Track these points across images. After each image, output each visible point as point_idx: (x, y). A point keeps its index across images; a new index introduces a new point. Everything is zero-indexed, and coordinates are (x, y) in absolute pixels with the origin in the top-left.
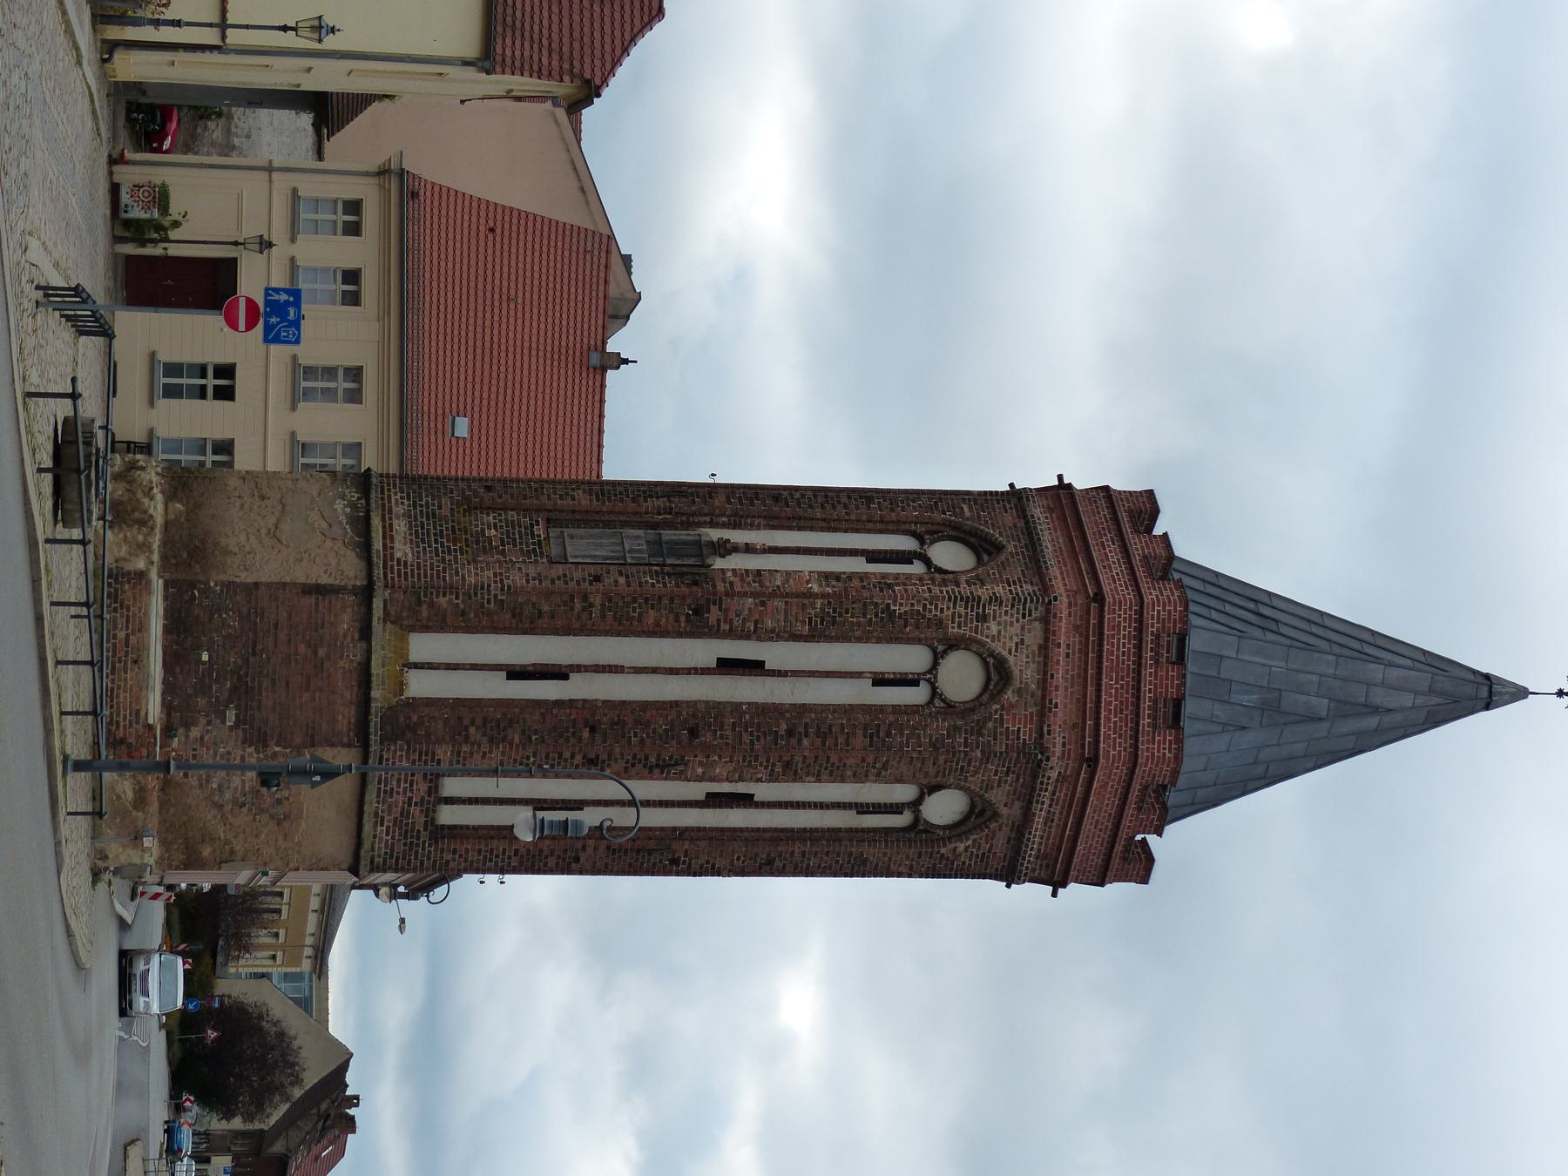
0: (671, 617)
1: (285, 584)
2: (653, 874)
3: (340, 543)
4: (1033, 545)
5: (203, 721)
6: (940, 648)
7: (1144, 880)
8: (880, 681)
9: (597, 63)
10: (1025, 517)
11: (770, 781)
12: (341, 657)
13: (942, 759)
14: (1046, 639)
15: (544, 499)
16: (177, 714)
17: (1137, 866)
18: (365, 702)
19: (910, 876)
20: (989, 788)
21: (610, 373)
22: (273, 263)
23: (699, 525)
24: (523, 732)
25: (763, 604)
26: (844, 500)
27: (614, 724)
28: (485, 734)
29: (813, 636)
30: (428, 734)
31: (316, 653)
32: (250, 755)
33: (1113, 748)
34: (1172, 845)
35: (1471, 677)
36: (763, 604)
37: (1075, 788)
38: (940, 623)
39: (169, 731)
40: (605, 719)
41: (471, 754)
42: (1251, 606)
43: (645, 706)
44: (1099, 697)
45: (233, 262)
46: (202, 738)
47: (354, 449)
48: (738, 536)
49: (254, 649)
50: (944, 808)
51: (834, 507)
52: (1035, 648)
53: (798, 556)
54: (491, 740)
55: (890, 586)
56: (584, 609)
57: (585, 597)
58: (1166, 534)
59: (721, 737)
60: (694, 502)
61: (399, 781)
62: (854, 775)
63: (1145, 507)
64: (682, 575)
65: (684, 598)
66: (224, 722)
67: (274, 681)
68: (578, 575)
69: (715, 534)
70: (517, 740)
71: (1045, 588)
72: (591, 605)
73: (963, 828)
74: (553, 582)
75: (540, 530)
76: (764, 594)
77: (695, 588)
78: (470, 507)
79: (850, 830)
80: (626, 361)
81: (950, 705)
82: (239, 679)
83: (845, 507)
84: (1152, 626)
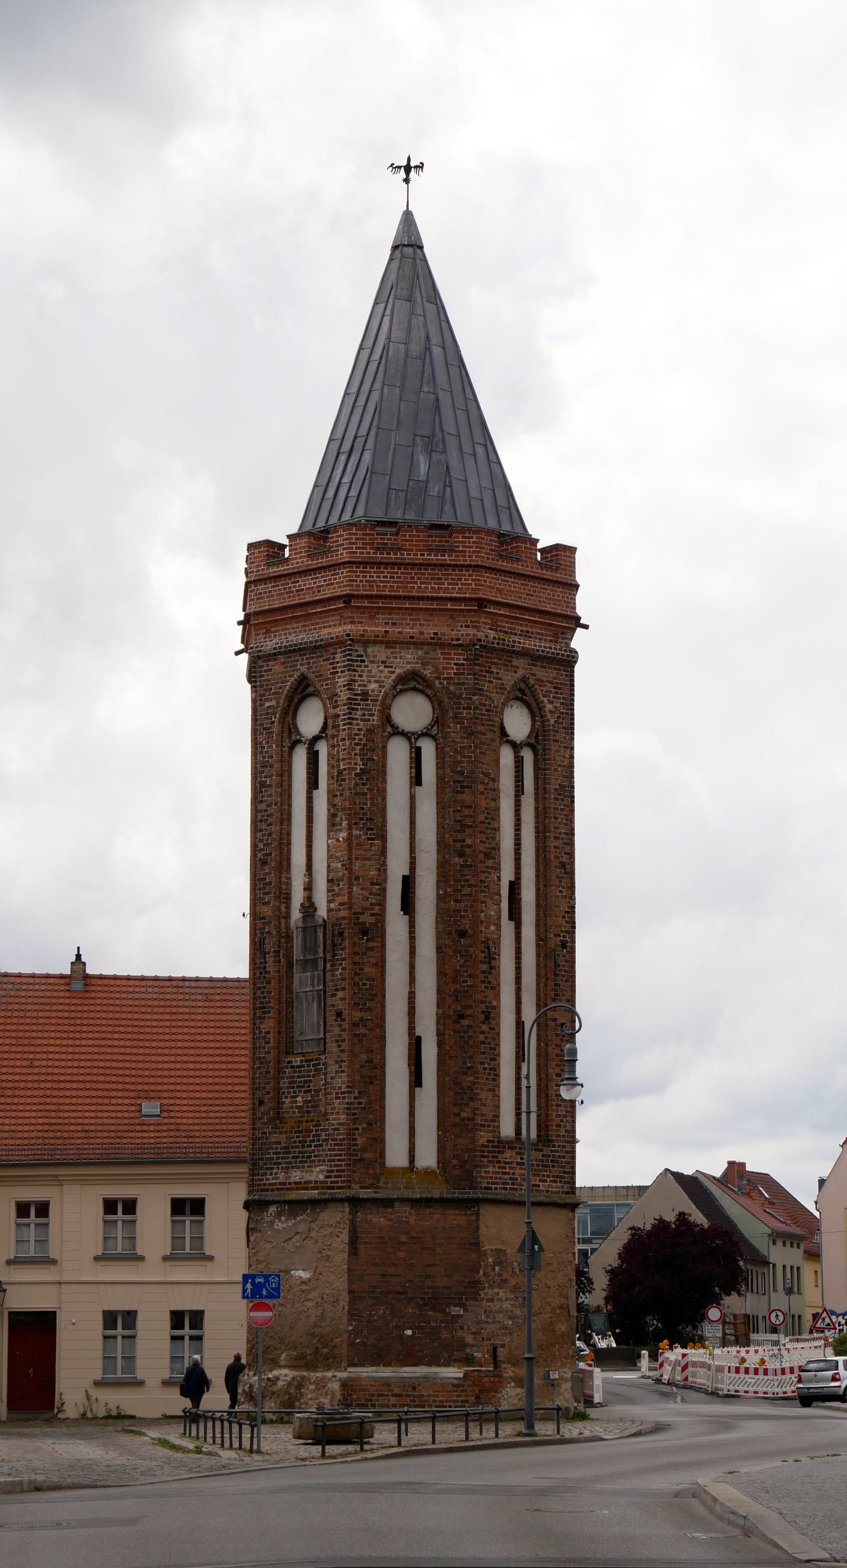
0: (370, 953)
1: (349, 1269)
2: (574, 962)
3: (313, 1225)
4: (300, 650)
5: (460, 1333)
6: (389, 729)
8: (417, 779)
10: (275, 654)
11: (500, 869)
12: (407, 1222)
13: (480, 728)
14: (381, 642)
16: (454, 1353)
17: (561, 557)
18: (443, 1202)
19: (572, 748)
20: (502, 687)
21: (90, 971)
22: (12, 1280)
23: (288, 928)
24: (465, 1073)
26: (263, 806)
27: (457, 1000)
28: (467, 1105)
29: (383, 836)
30: (468, 1151)
31: (404, 1243)
32: (486, 1294)
33: (466, 586)
34: (544, 532)
35: (396, 263)
36: (357, 878)
37: (501, 615)
38: (370, 731)
39: (469, 1360)
40: (453, 1007)
41: (483, 1115)
42: (343, 458)
43: (441, 974)
44: (428, 598)
46: (474, 1333)
48: (298, 897)
49: (402, 1293)
50: (517, 723)
51: (270, 815)
52: (389, 651)
53: (314, 850)
54: (472, 1099)
55: (340, 773)
56: (365, 1025)
57: (355, 1024)
58: (289, 537)
59: (465, 911)
60: (269, 932)
61: (504, 1173)
62: (494, 800)
63: (264, 553)
64: (334, 945)
65: (354, 944)
66: (460, 1316)
67: (427, 1277)
68: (336, 1030)
69: (296, 915)
70: (471, 1079)
71: (338, 643)
72: (362, 1020)
73: (534, 706)
74: (343, 1051)
75: (297, 1061)
76: (350, 878)
77: (346, 935)
78: (278, 1117)
79: (537, 800)
80: (78, 956)
81: (437, 721)
82: (427, 1305)
83: (269, 806)
84: (370, 553)
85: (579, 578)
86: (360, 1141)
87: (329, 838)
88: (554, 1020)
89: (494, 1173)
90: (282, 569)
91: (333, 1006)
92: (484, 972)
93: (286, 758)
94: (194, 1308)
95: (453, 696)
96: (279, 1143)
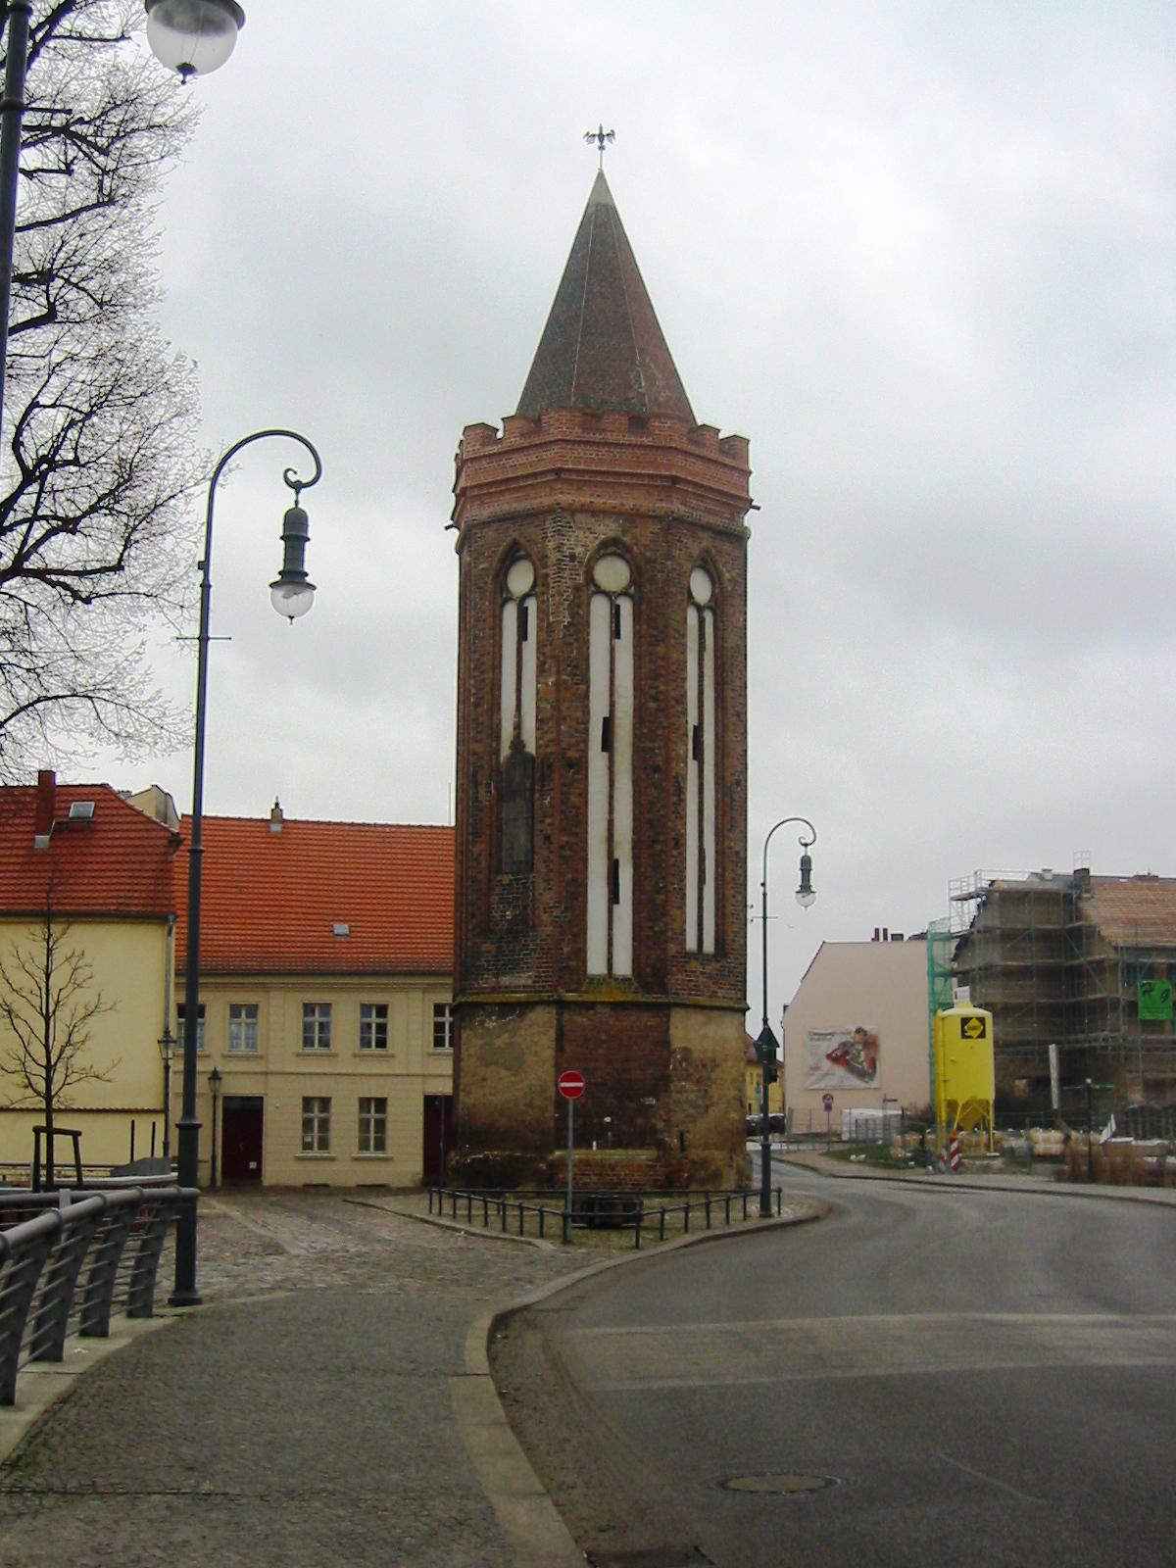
6: (592, 588)
7: (748, 441)
8: (616, 633)
9: (153, 835)
10: (489, 522)
14: (586, 511)
15: (481, 876)
16: (645, 1137)
17: (736, 447)
22: (228, 1070)
24: (658, 893)
25: (564, 718)
36: (564, 718)
45: (227, 1099)
47: (439, 1010)
50: (701, 588)
51: (484, 663)
56: (571, 849)
57: (562, 847)
66: (652, 1106)
68: (545, 853)
71: (550, 511)
74: (551, 871)
80: (277, 805)
81: (633, 581)
83: (482, 655)
84: (577, 433)
85: (751, 467)
86: (566, 950)
87: (538, 682)
88: (730, 848)
89: (683, 980)
90: (495, 449)
91: (542, 831)
92: (674, 804)
93: (498, 612)
94: (379, 1095)
95: (650, 561)
96: (489, 952)
